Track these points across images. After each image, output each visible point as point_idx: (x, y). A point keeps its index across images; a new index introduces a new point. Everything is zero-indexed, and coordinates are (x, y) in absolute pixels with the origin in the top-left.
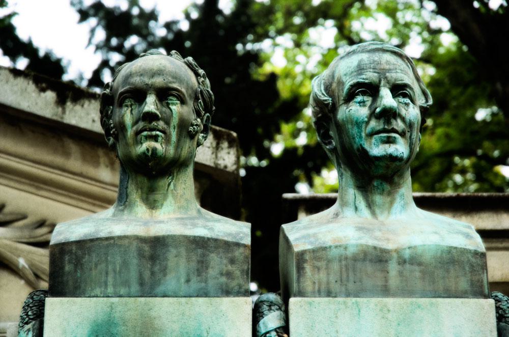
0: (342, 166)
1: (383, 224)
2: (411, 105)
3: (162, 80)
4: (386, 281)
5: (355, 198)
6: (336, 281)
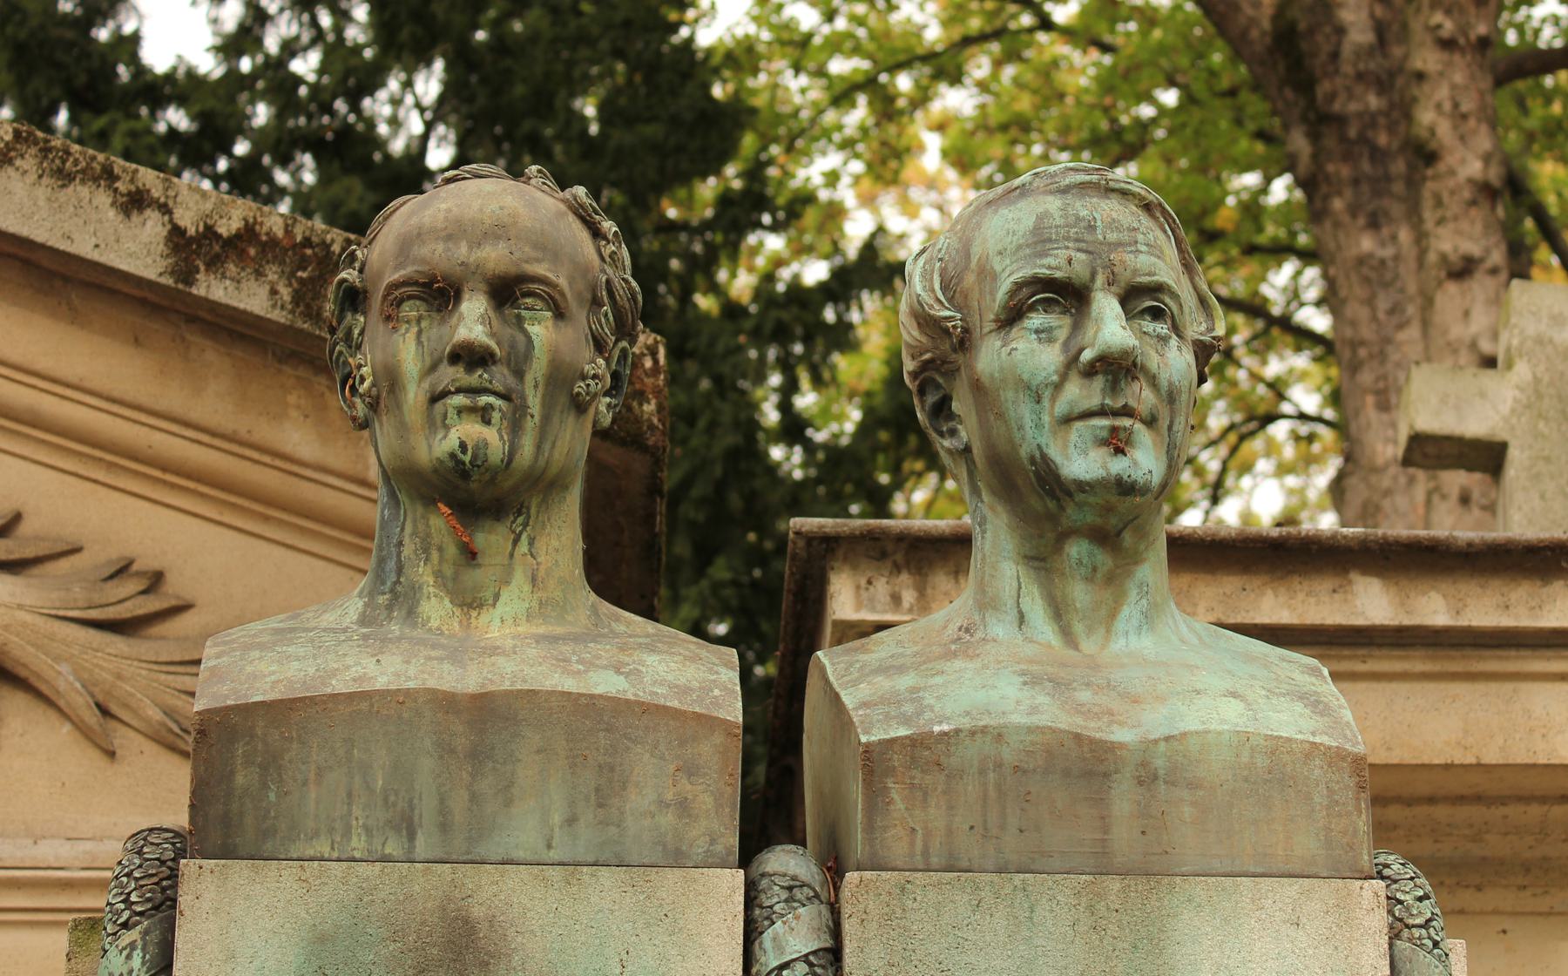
0: (986, 496)
1: (1095, 666)
2: (1174, 341)
3: (507, 252)
4: (1106, 830)
5: (1020, 588)
6: (972, 828)
